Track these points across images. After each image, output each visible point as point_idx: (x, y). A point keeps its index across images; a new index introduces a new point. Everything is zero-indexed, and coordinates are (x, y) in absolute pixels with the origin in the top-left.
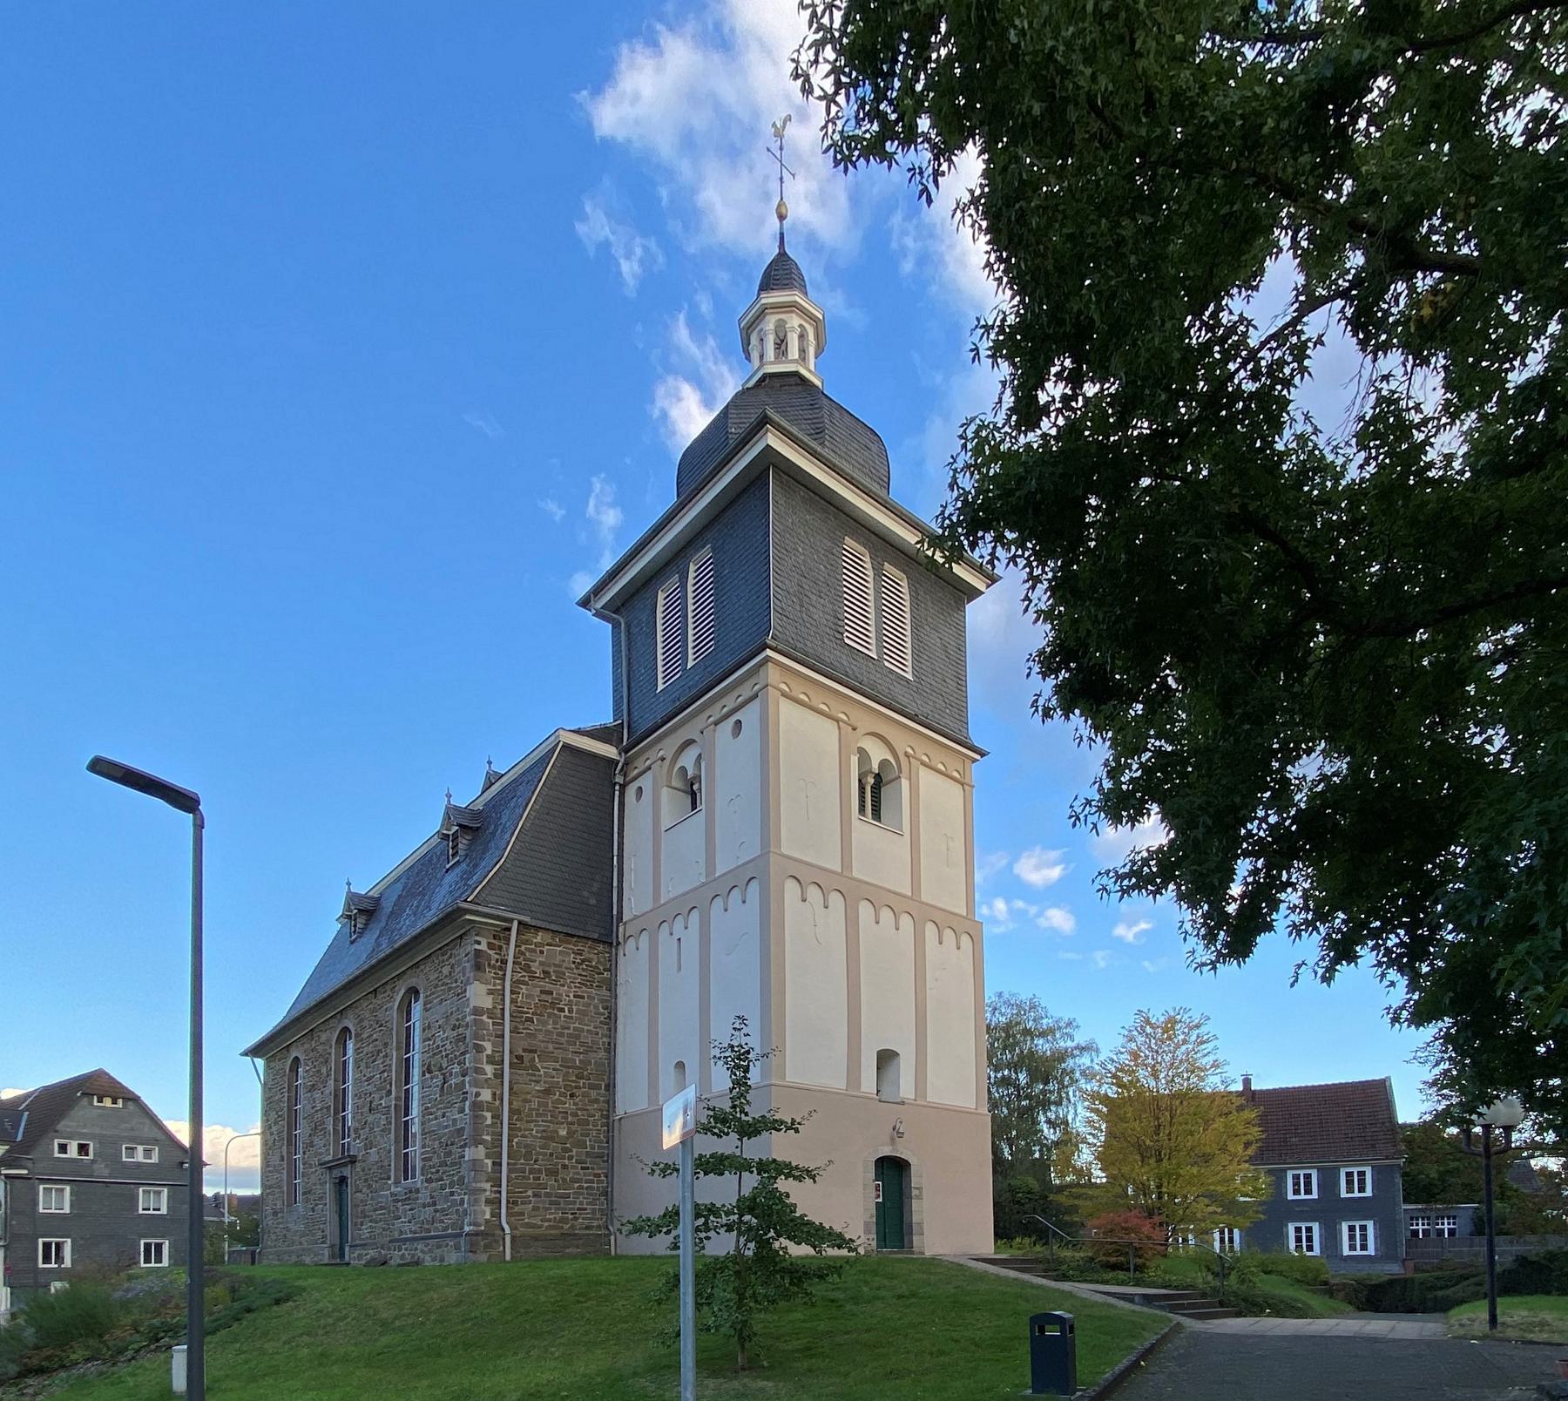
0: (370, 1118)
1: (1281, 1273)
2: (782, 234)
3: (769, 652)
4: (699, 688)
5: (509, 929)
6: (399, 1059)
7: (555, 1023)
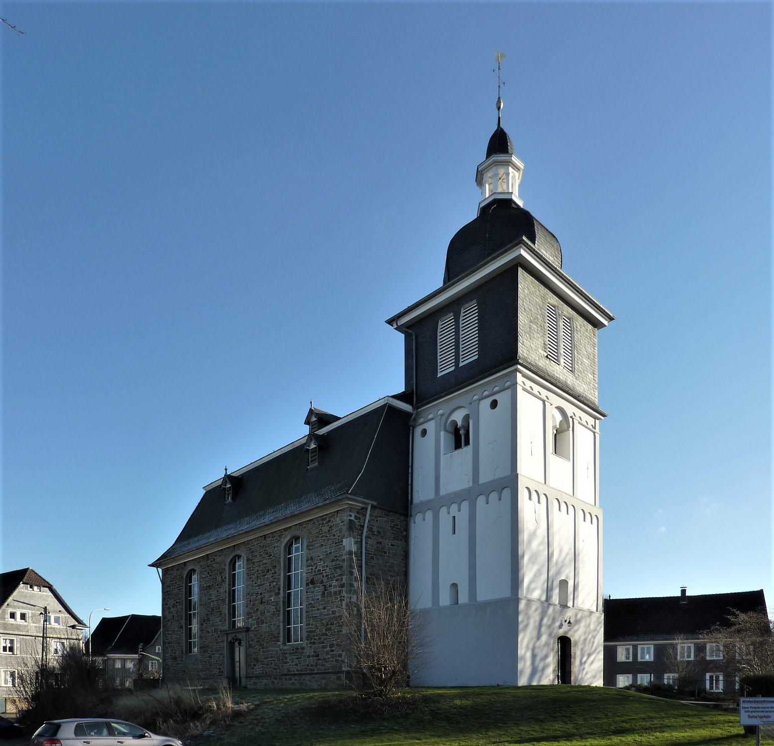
0: (261, 607)
1: (294, 675)
2: (499, 118)
3: (519, 367)
4: (465, 377)
5: (367, 509)
6: (285, 575)
7: (383, 559)
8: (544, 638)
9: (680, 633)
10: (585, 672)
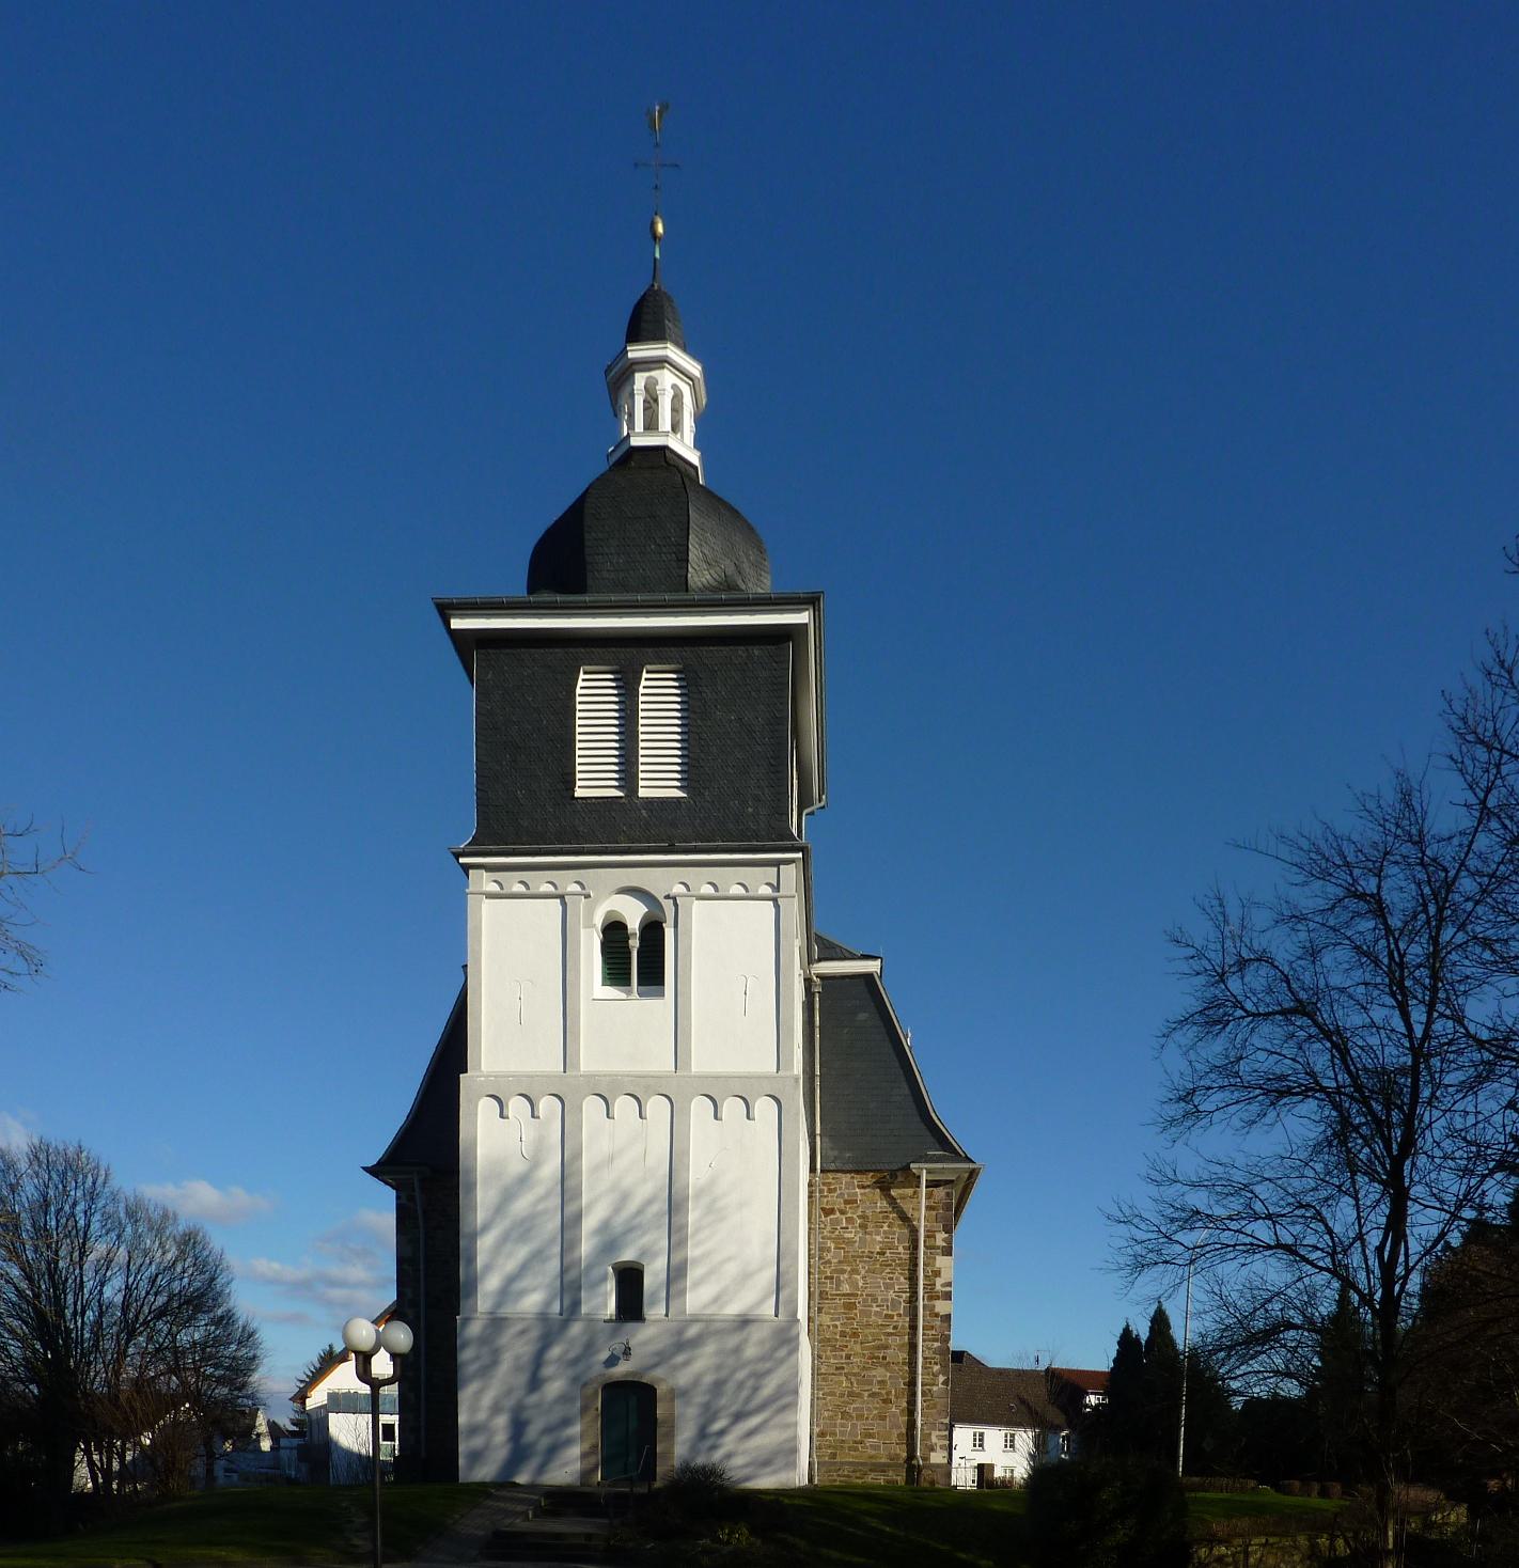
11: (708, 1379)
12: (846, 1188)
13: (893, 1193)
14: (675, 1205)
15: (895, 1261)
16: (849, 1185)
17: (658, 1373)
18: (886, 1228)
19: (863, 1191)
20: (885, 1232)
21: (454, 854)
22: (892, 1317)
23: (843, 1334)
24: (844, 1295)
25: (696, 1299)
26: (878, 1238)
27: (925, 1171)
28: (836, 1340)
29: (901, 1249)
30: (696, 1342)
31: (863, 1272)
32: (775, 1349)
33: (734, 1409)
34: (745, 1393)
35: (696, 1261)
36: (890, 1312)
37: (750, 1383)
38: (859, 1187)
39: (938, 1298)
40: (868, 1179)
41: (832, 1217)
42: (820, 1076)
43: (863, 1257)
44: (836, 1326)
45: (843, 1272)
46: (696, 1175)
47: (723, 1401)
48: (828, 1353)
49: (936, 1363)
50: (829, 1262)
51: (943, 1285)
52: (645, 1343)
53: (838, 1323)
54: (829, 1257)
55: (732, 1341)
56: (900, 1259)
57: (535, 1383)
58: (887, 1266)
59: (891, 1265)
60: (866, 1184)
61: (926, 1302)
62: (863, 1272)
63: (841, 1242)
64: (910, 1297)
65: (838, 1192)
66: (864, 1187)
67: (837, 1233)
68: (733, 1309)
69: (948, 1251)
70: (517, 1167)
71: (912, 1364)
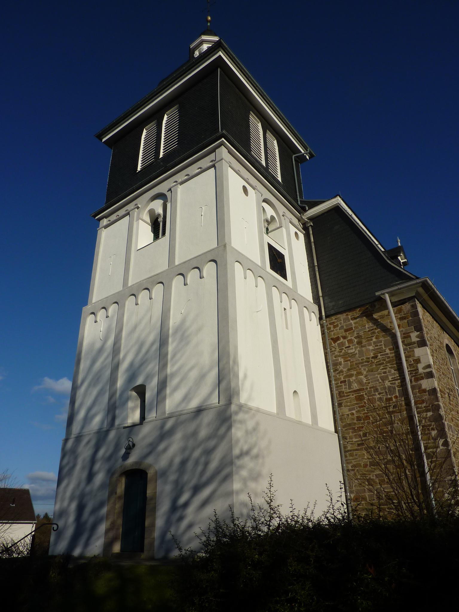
8: (99, 478)
9: (318, 526)
10: (184, 524)
11: (177, 460)
12: (344, 322)
13: (375, 316)
14: (163, 341)
15: (384, 360)
16: (346, 320)
17: (150, 460)
18: (374, 340)
19: (355, 321)
20: (374, 343)
21: (93, 216)
22: (391, 399)
23: (359, 419)
24: (355, 391)
25: (171, 404)
26: (371, 348)
27: (387, 296)
28: (355, 423)
29: (388, 351)
30: (171, 432)
31: (365, 373)
32: (218, 429)
33: (194, 482)
34: (200, 468)
35: (173, 375)
36: (389, 397)
37: (203, 460)
38: (352, 319)
39: (422, 378)
40: (357, 313)
41: (338, 342)
42: (318, 266)
43: (363, 363)
44: (353, 414)
45: (351, 376)
46: (173, 322)
47: (186, 477)
48: (351, 434)
49: (433, 429)
50: (342, 371)
51: (424, 368)
52: (144, 438)
53: (354, 412)
54: (341, 368)
55: (191, 427)
56: (389, 357)
57: (91, 476)
58: (380, 364)
59: (383, 363)
60: (356, 316)
61: (414, 383)
62: (365, 373)
63: (346, 356)
64: (401, 382)
65: (340, 326)
66: (355, 318)
67: (343, 351)
68: (194, 404)
69: (422, 343)
70: (98, 345)
71: (414, 432)
